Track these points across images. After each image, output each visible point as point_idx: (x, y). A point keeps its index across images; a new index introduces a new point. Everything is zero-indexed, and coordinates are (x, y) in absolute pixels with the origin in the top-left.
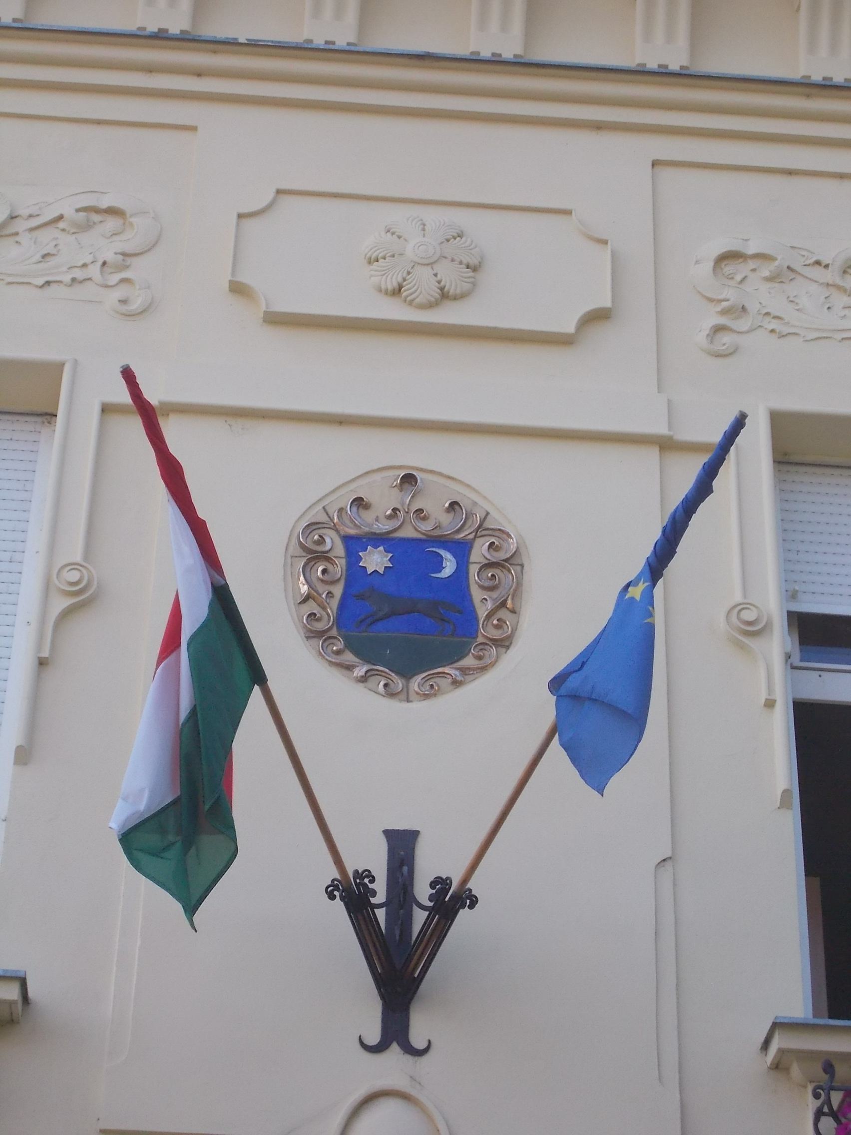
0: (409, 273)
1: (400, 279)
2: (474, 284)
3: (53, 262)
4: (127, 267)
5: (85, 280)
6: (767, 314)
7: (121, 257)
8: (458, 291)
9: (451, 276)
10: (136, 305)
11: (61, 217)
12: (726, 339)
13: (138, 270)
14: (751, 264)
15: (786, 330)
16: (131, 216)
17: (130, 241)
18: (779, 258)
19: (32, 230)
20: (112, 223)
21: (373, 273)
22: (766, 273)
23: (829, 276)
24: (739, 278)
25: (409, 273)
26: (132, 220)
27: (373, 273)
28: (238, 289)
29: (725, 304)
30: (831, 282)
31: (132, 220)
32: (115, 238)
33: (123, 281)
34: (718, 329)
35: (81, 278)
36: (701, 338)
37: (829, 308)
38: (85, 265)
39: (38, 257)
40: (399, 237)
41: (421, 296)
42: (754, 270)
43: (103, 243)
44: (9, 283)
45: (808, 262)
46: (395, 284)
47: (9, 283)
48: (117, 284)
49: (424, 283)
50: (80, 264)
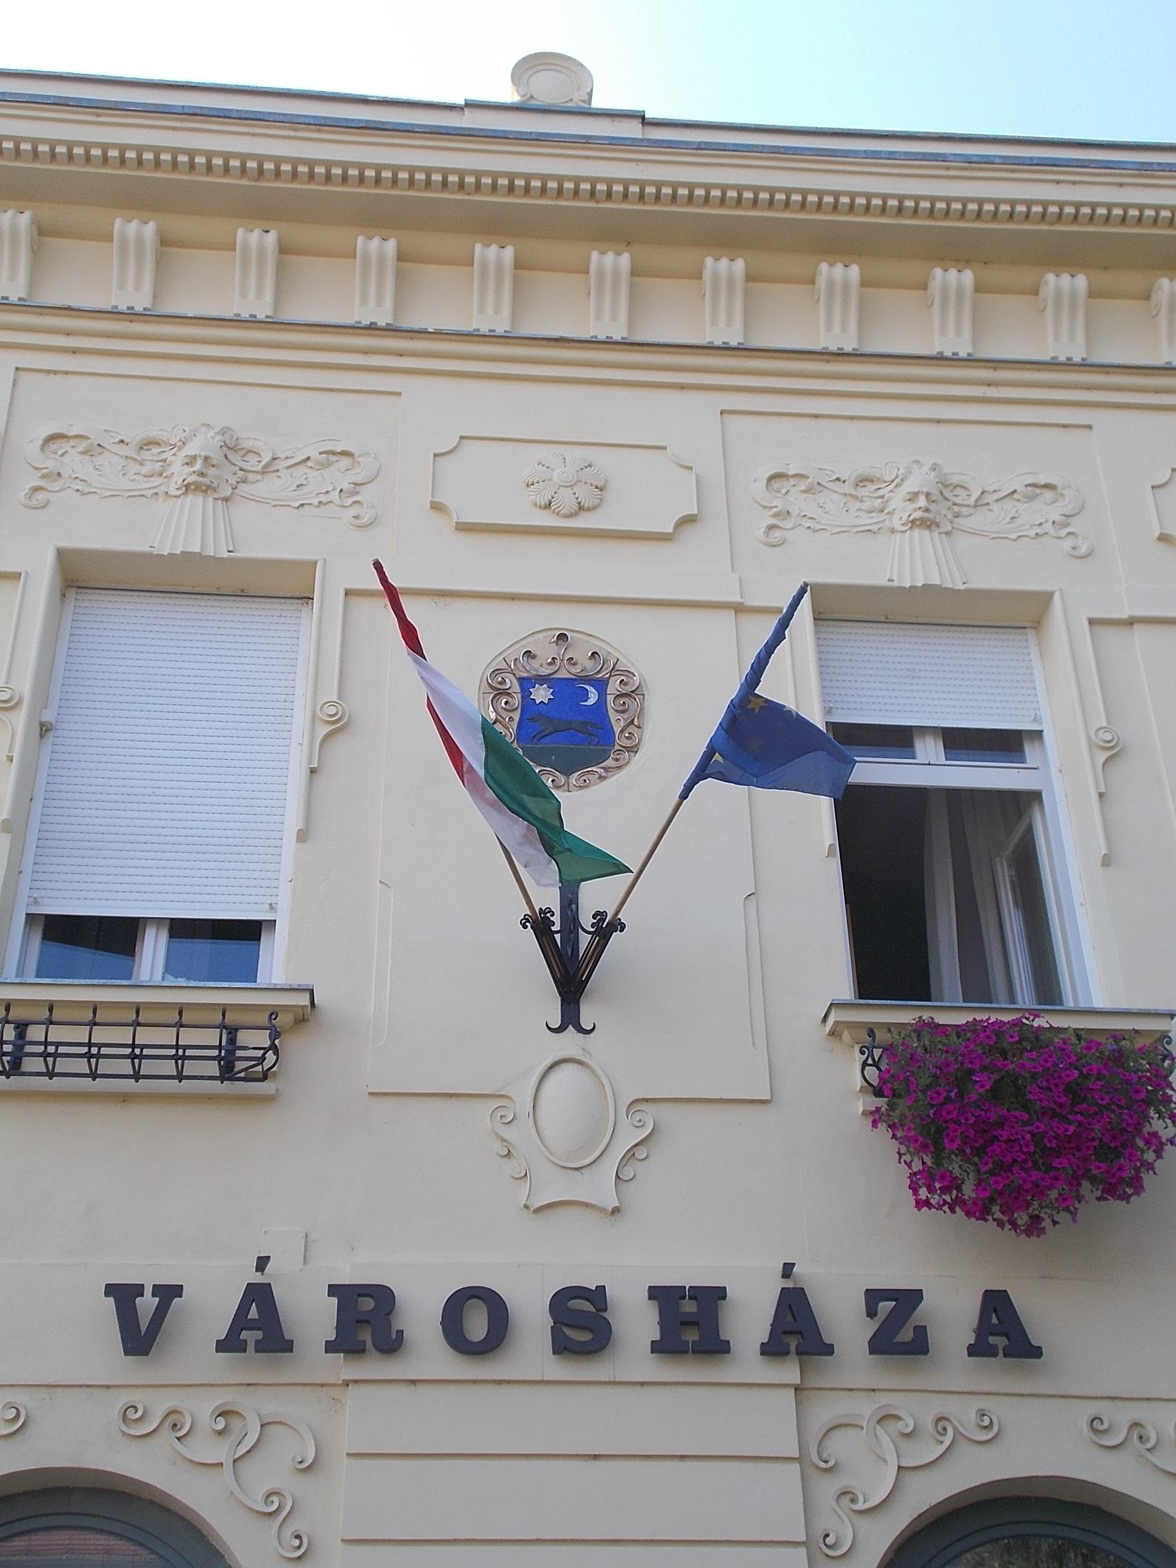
4: (775, 515)
9: (585, 494)
10: (1083, 550)
12: (40, 496)
14: (792, 482)
17: (359, 474)
23: (847, 488)
38: (327, 492)
49: (566, 500)
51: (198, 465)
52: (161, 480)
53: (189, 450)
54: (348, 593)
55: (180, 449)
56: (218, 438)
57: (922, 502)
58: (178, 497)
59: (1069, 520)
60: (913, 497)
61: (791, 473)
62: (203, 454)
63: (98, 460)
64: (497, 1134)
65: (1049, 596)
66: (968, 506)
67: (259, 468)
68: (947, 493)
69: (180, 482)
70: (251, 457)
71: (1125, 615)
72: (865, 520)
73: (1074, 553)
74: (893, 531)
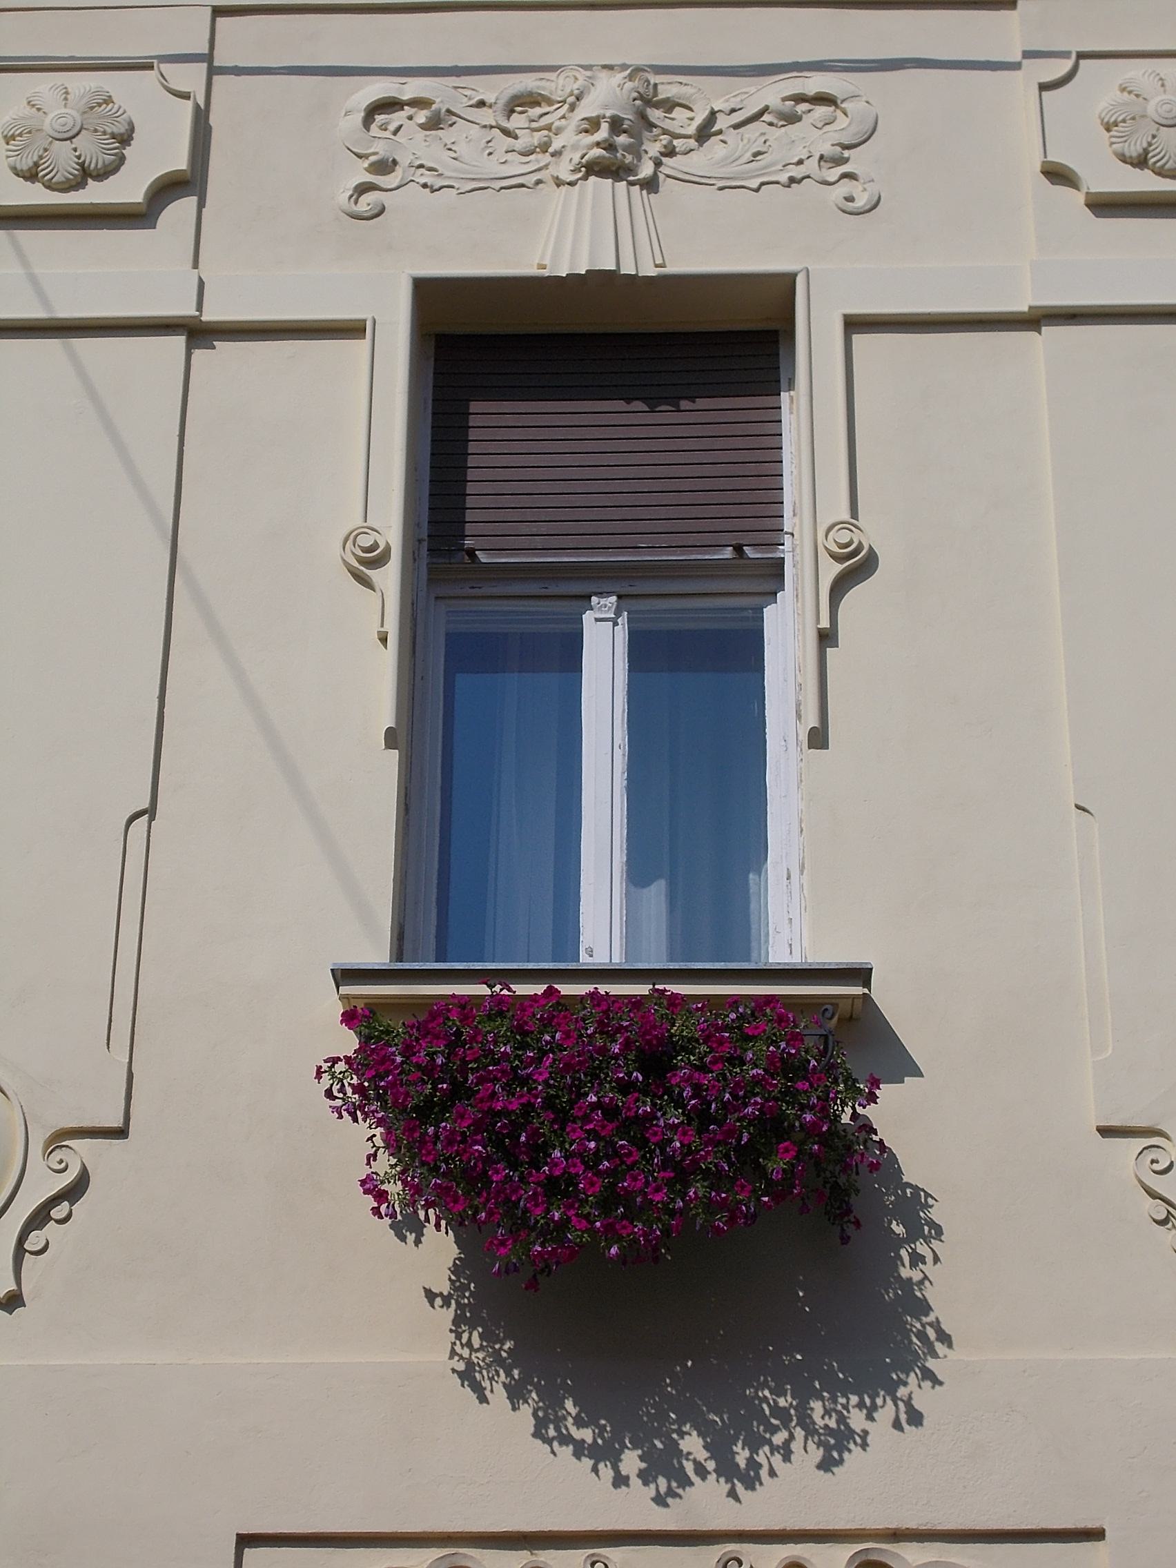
0: (1154, 137)
1: (1145, 145)
2: (122, 159)
3: (764, 160)
4: (846, 160)
5: (803, 178)
6: (421, 166)
7: (839, 149)
8: (105, 166)
9: (92, 149)
10: (861, 202)
11: (765, 110)
12: (370, 198)
13: (857, 162)
14: (408, 110)
15: (438, 183)
16: (843, 101)
17: (844, 127)
18: (438, 100)
19: (736, 126)
20: (822, 111)
21: (1114, 140)
22: (422, 120)
23: (486, 116)
24: (392, 127)
25: (1154, 137)
26: (843, 106)
27: (1114, 140)
28: (1057, 175)
29: (373, 158)
30: (494, 124)
31: (843, 106)
32: (827, 128)
33: (845, 176)
34: (363, 189)
35: (800, 176)
36: (343, 197)
37: (490, 154)
38: (800, 162)
39: (748, 156)
40: (1137, 96)
41: (1171, 162)
42: (410, 118)
43: (814, 136)
44: (721, 189)
45: (471, 103)
46: (31, 164)
47: (721, 189)
48: (803, 178)
49: (63, 160)
50: (795, 160)
51: (603, 133)
52: (546, 158)
53: (588, 109)
54: (854, 325)
55: (572, 108)
56: (629, 85)
57: (603, 133)
58: (571, 184)
59: (846, 153)
60: (593, 124)
61: (405, 98)
62: (608, 113)
63: (446, 135)
64: (1141, 1182)
65: (790, 279)
66: (689, 137)
67: (691, 129)
68: (655, 115)
69: (576, 158)
70: (678, 113)
71: (1021, 305)
72: (517, 166)
73: (850, 206)
74: (559, 183)
